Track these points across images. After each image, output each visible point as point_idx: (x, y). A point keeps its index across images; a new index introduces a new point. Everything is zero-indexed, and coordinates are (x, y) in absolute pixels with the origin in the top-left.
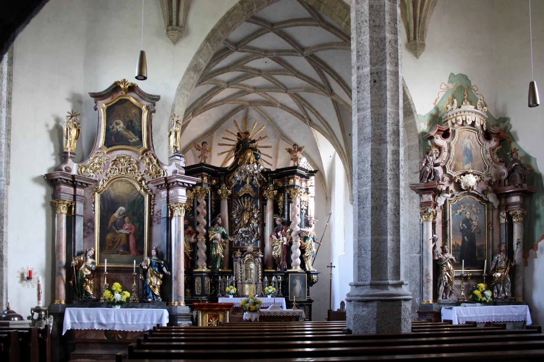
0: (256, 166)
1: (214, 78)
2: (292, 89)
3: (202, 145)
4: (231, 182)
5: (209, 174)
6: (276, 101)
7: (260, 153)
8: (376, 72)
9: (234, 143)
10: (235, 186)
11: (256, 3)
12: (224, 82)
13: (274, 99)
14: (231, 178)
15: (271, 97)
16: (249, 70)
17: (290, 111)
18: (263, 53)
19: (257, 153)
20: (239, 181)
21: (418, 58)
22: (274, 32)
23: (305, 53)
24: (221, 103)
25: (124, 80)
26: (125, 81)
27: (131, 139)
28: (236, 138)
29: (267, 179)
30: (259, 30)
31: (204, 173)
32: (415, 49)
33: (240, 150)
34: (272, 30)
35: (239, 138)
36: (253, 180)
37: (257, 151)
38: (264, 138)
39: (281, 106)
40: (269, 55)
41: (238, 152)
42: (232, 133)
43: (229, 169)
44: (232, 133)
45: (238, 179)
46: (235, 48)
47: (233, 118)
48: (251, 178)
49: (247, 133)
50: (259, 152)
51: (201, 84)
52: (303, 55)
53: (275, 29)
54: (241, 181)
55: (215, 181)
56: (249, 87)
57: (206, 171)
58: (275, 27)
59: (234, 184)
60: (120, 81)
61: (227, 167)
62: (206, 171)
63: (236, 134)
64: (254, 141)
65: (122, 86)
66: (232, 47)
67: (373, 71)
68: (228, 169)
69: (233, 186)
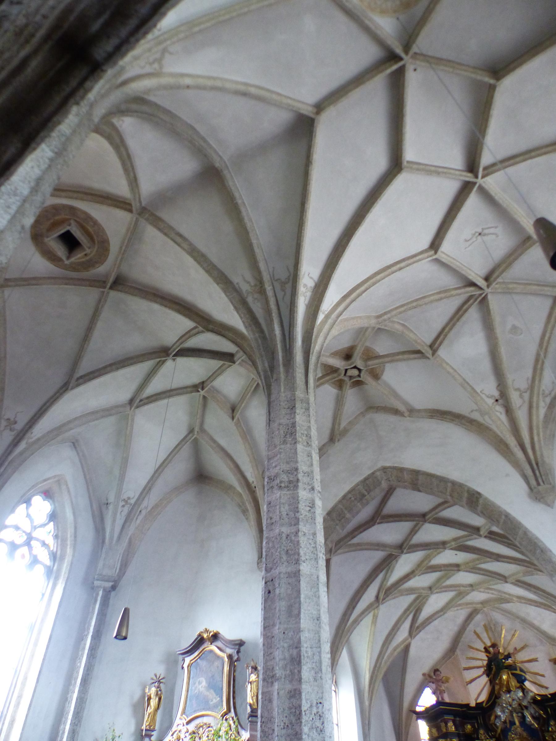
0: (520, 694)
1: (400, 588)
2: (510, 576)
3: (434, 674)
4: (495, 725)
5: (455, 717)
6: (509, 594)
7: (524, 672)
8: (271, 579)
9: (485, 663)
10: (502, 730)
11: (346, 509)
12: (423, 589)
13: (505, 593)
14: (493, 718)
15: (499, 591)
16: (443, 569)
17: (536, 604)
18: (441, 546)
19: (518, 672)
20: (505, 722)
21: (552, 508)
22: (430, 523)
23: (482, 533)
24: (442, 613)
25: (206, 629)
26: (207, 631)
27: (212, 701)
28: (483, 656)
29: (546, 712)
30: (415, 526)
31: (446, 717)
32: (542, 498)
33: (493, 673)
34: (425, 521)
35: (488, 655)
36: (523, 717)
37: (516, 670)
38: (523, 648)
39: (519, 600)
40: (449, 547)
41: (491, 676)
42: (477, 650)
43: (486, 704)
44: (477, 650)
45: (503, 719)
46: (400, 551)
47: (471, 627)
48: (520, 714)
49: (494, 645)
50: (521, 670)
51: (386, 599)
52: (480, 536)
53: (428, 519)
54: (508, 721)
55: (469, 726)
56: (463, 586)
57: (449, 712)
58: (427, 517)
59: (500, 728)
60: (203, 631)
61: (483, 702)
62: (449, 712)
63: (483, 650)
64: (508, 656)
65: (205, 636)
66: (395, 552)
67: (268, 579)
68: (484, 704)
69: (499, 731)
